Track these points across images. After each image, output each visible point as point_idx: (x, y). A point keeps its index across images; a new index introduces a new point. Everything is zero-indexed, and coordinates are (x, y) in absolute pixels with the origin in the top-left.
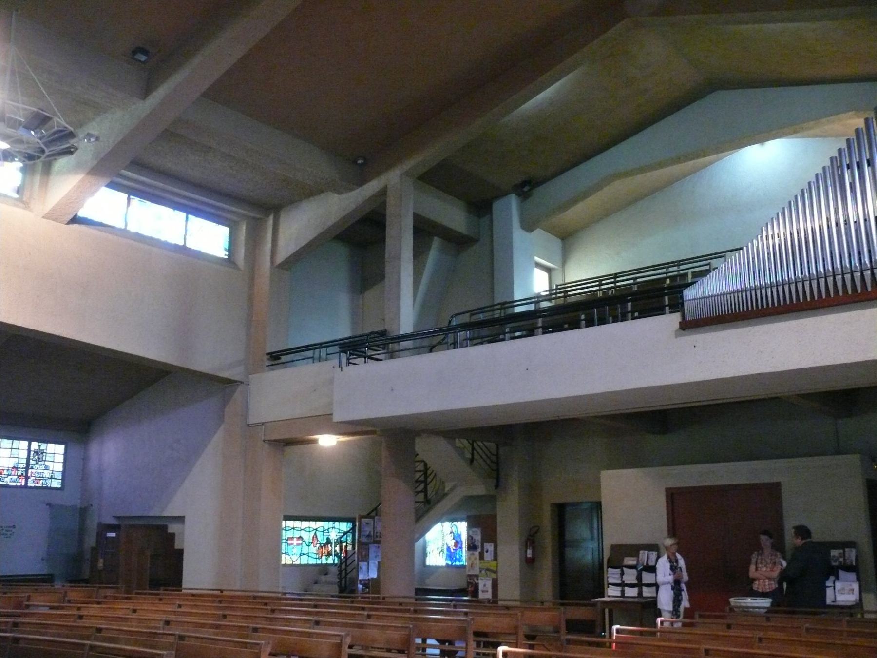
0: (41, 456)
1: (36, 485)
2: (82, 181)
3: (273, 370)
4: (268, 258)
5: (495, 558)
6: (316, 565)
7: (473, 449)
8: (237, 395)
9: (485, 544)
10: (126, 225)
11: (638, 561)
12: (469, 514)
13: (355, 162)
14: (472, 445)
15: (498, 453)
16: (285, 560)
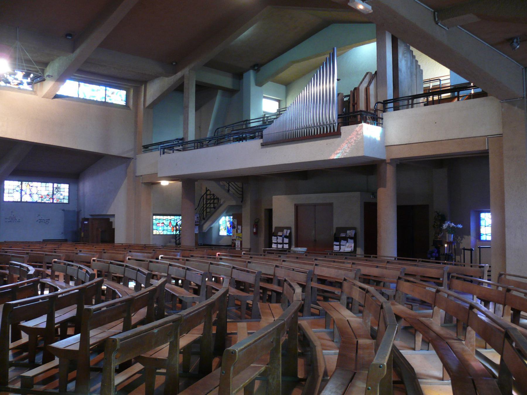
0: (59, 189)
1: (58, 202)
2: (54, 84)
3: (146, 153)
4: (142, 104)
5: (241, 232)
6: (171, 235)
7: (229, 185)
8: (131, 164)
9: (238, 226)
10: (79, 96)
11: (283, 234)
12: (233, 213)
13: (172, 64)
14: (229, 184)
15: (242, 187)
16: (155, 232)
